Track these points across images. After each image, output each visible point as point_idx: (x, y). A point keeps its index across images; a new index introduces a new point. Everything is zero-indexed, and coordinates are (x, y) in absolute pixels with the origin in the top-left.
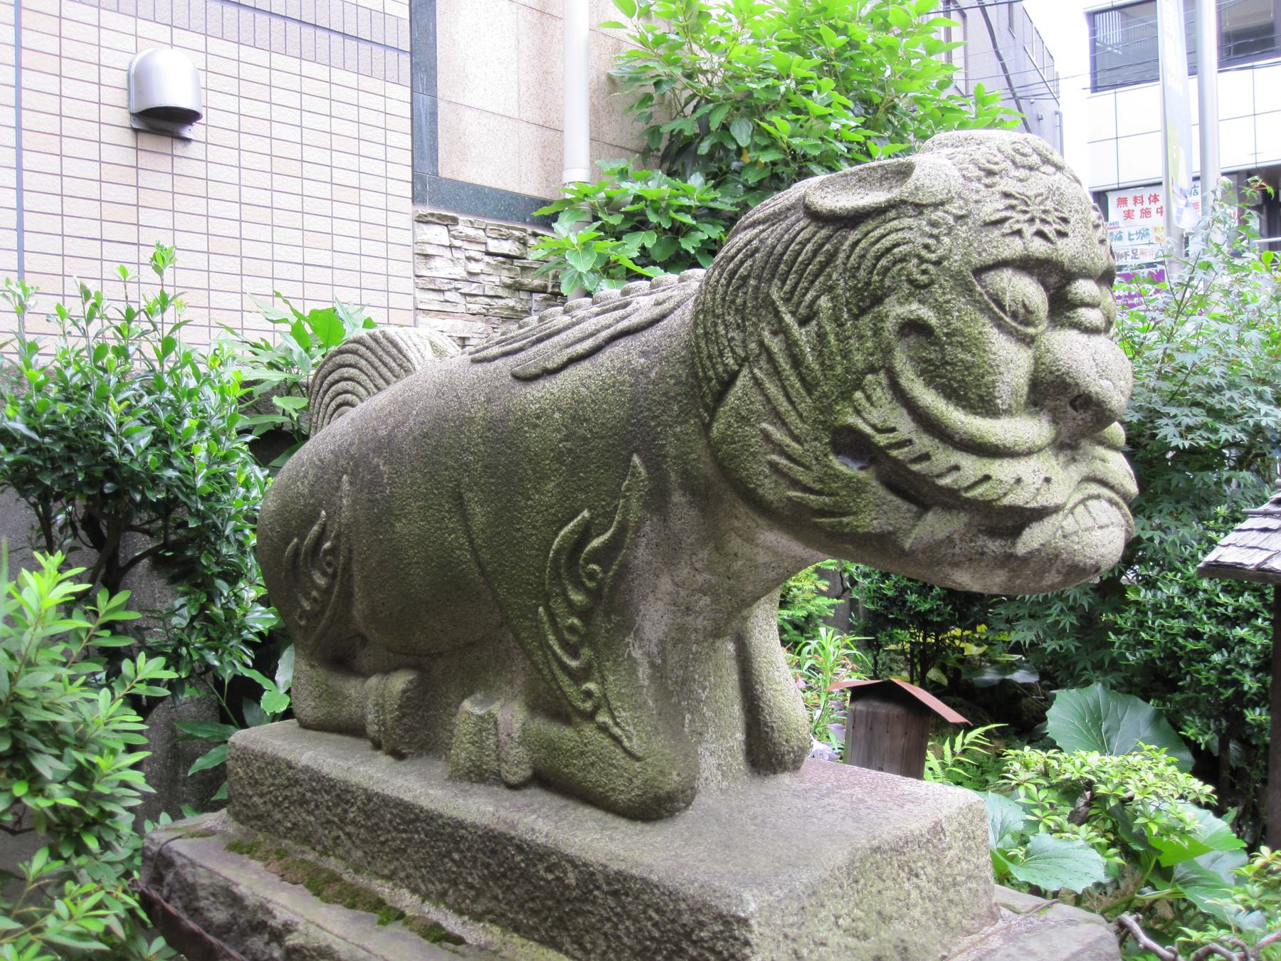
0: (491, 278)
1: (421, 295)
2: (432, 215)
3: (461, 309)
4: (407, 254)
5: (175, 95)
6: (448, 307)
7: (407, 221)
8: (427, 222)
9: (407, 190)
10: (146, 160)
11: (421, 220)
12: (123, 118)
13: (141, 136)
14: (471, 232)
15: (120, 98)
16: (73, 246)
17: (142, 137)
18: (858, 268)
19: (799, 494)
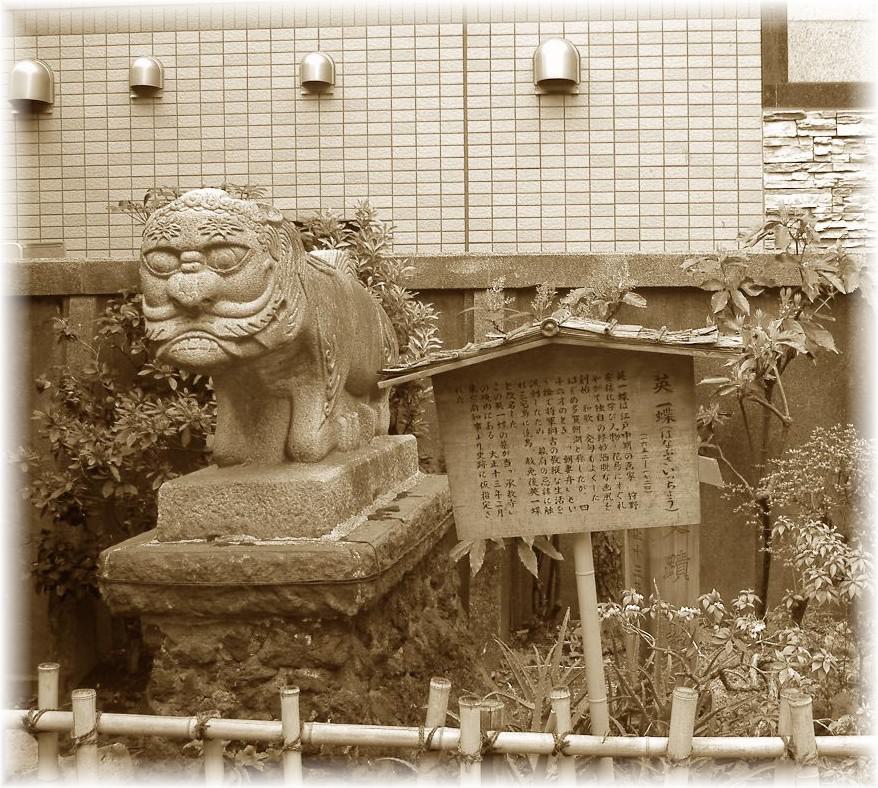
0: (840, 157)
1: (768, 178)
2: (778, 114)
3: (808, 185)
4: (757, 147)
5: (555, 70)
6: (795, 185)
7: (757, 122)
8: (775, 121)
9: (758, 98)
10: (545, 113)
11: (767, 120)
12: (531, 88)
13: (542, 98)
14: (819, 122)
15: (529, 76)
16: (498, 175)
17: (543, 99)
18: (157, 390)
19: (289, 541)
